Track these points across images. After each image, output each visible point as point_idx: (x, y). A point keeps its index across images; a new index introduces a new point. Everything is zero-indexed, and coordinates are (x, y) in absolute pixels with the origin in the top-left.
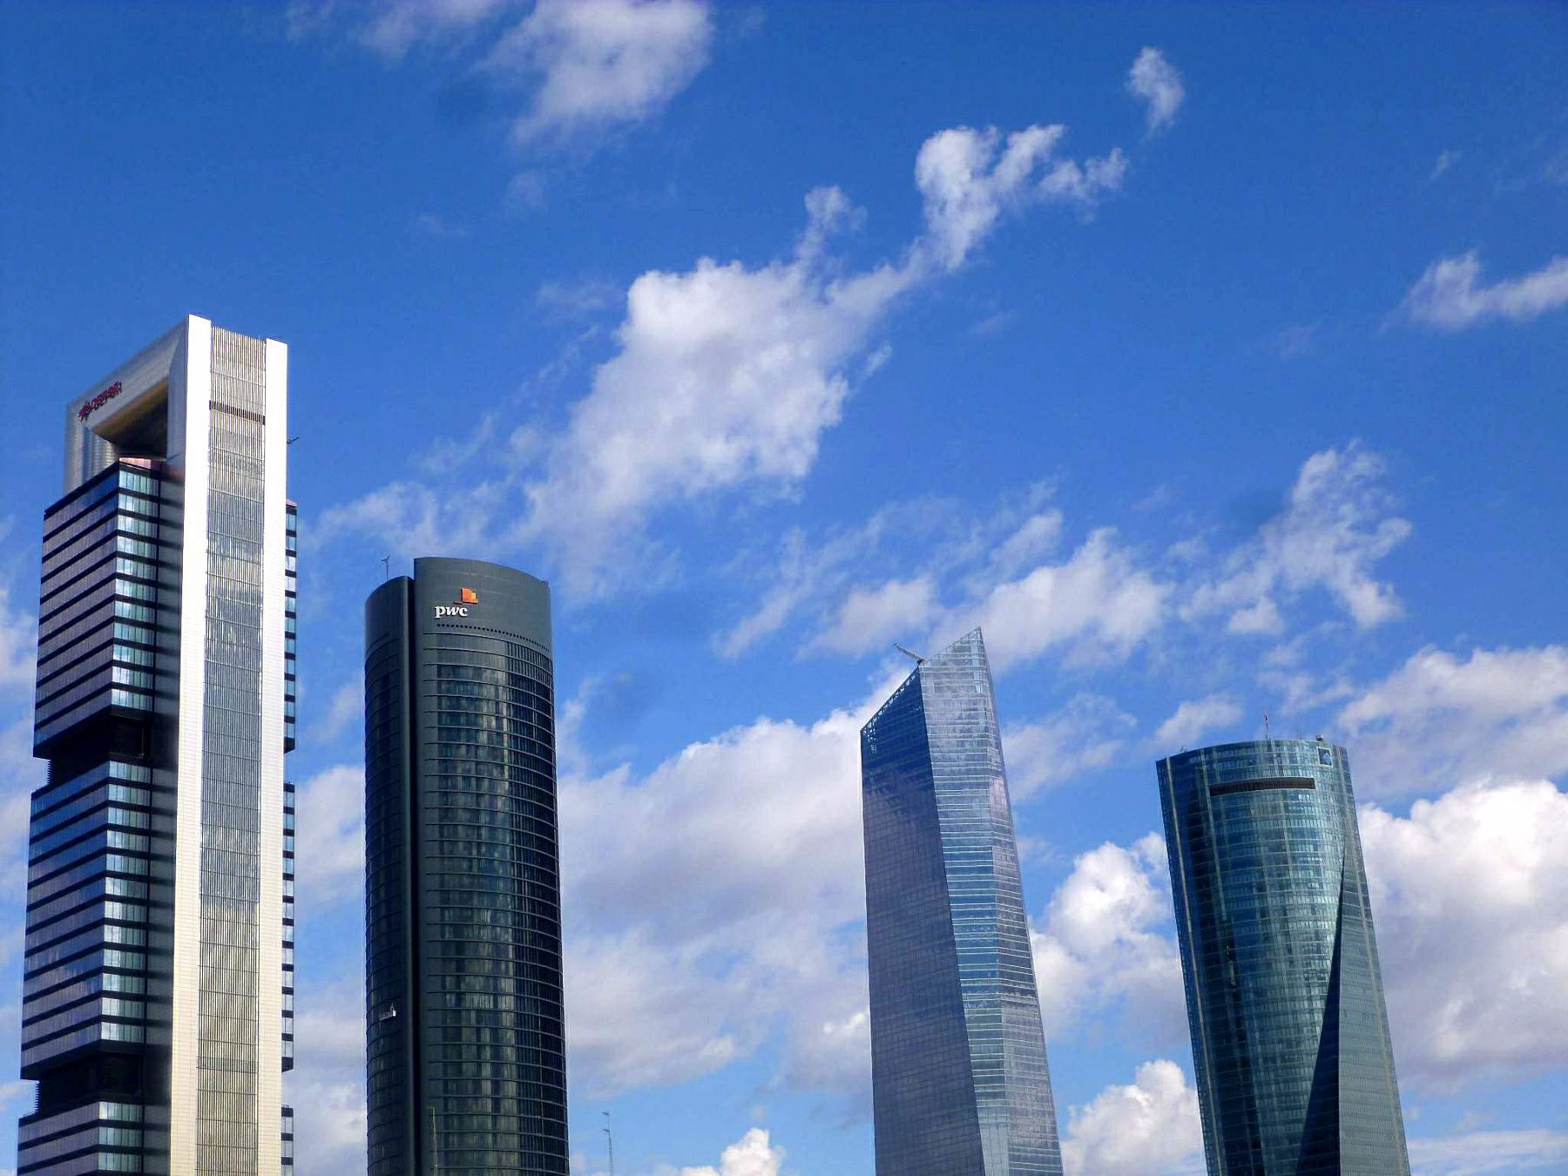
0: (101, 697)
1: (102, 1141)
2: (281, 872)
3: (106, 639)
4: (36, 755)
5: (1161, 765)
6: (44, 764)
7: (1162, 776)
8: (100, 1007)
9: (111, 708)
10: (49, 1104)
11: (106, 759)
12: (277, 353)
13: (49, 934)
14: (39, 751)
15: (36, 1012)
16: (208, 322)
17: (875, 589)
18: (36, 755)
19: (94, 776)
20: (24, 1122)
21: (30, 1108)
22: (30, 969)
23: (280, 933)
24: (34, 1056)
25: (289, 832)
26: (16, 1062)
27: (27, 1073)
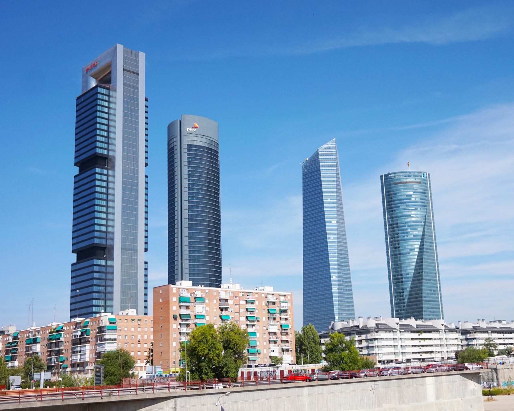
0: (93, 189)
1: (95, 277)
2: (144, 313)
3: (94, 134)
4: (72, 252)
5: (381, 176)
6: (78, 168)
7: (382, 179)
8: (95, 208)
9: (96, 153)
10: (81, 171)
11: (95, 167)
12: (142, 56)
13: (80, 214)
14: (76, 165)
15: (77, 204)
16: (123, 46)
17: (305, 167)
18: (72, 252)
19: (92, 172)
20: (73, 265)
21: (75, 261)
22: (75, 217)
23: (144, 120)
24: (76, 247)
25: (146, 195)
26: (70, 248)
27: (73, 252)
